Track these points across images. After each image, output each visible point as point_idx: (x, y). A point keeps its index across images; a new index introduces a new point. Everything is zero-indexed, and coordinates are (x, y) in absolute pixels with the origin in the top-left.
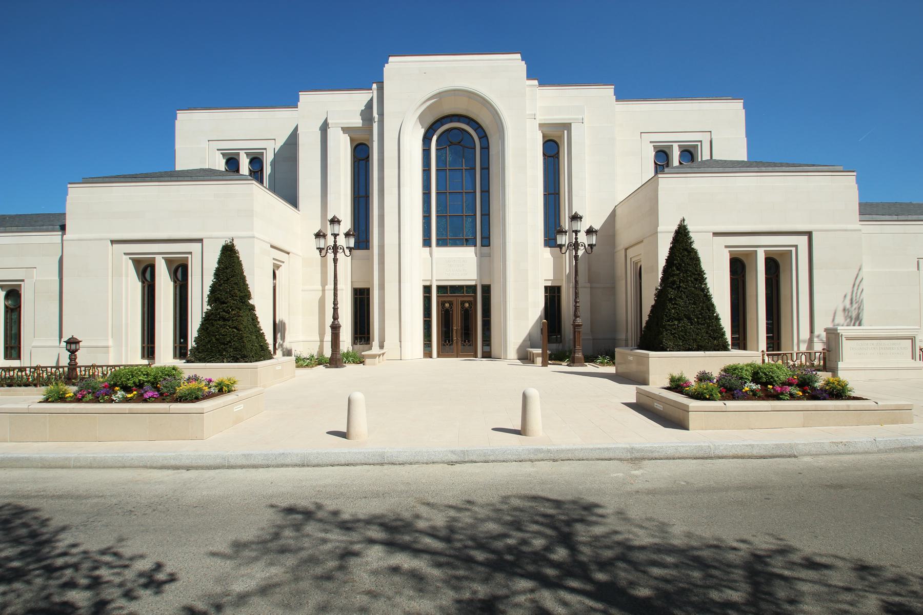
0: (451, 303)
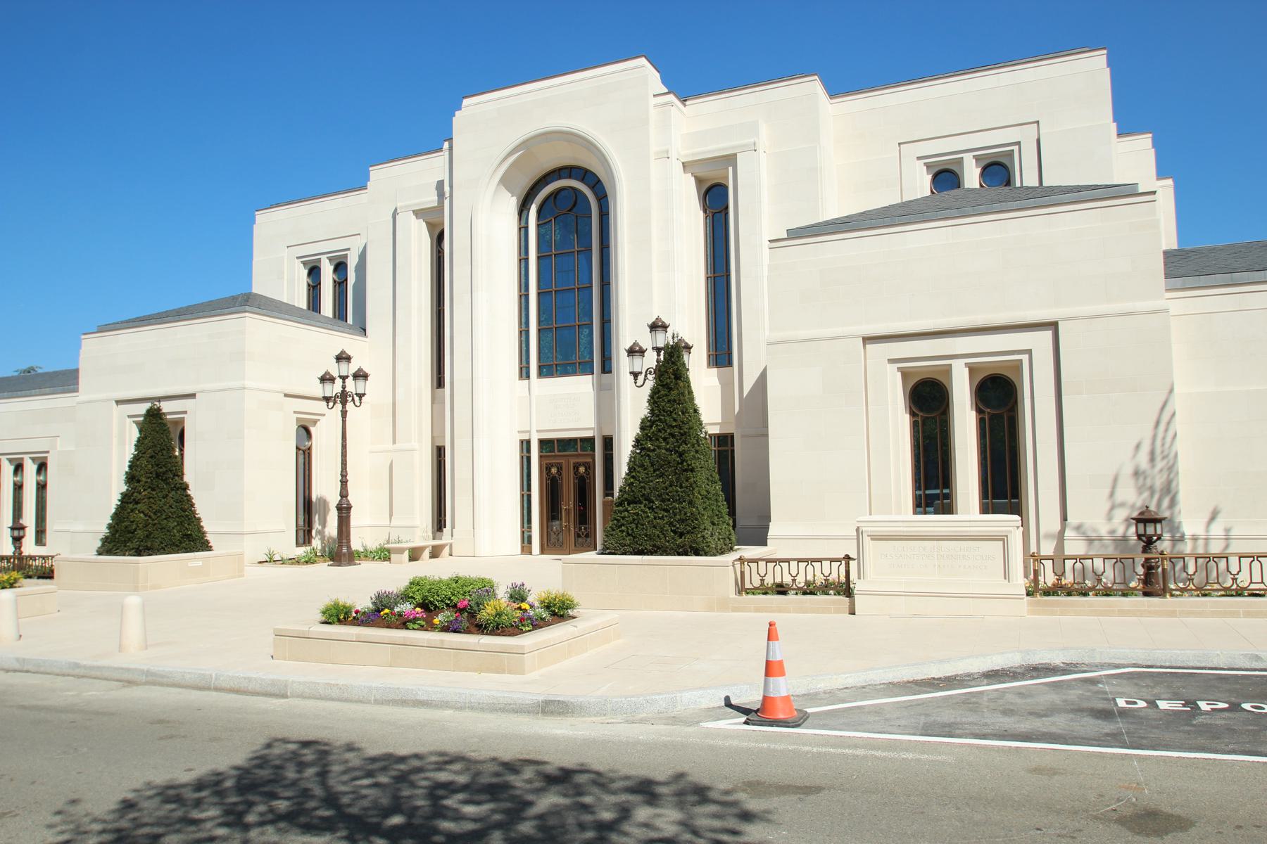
0: (560, 469)
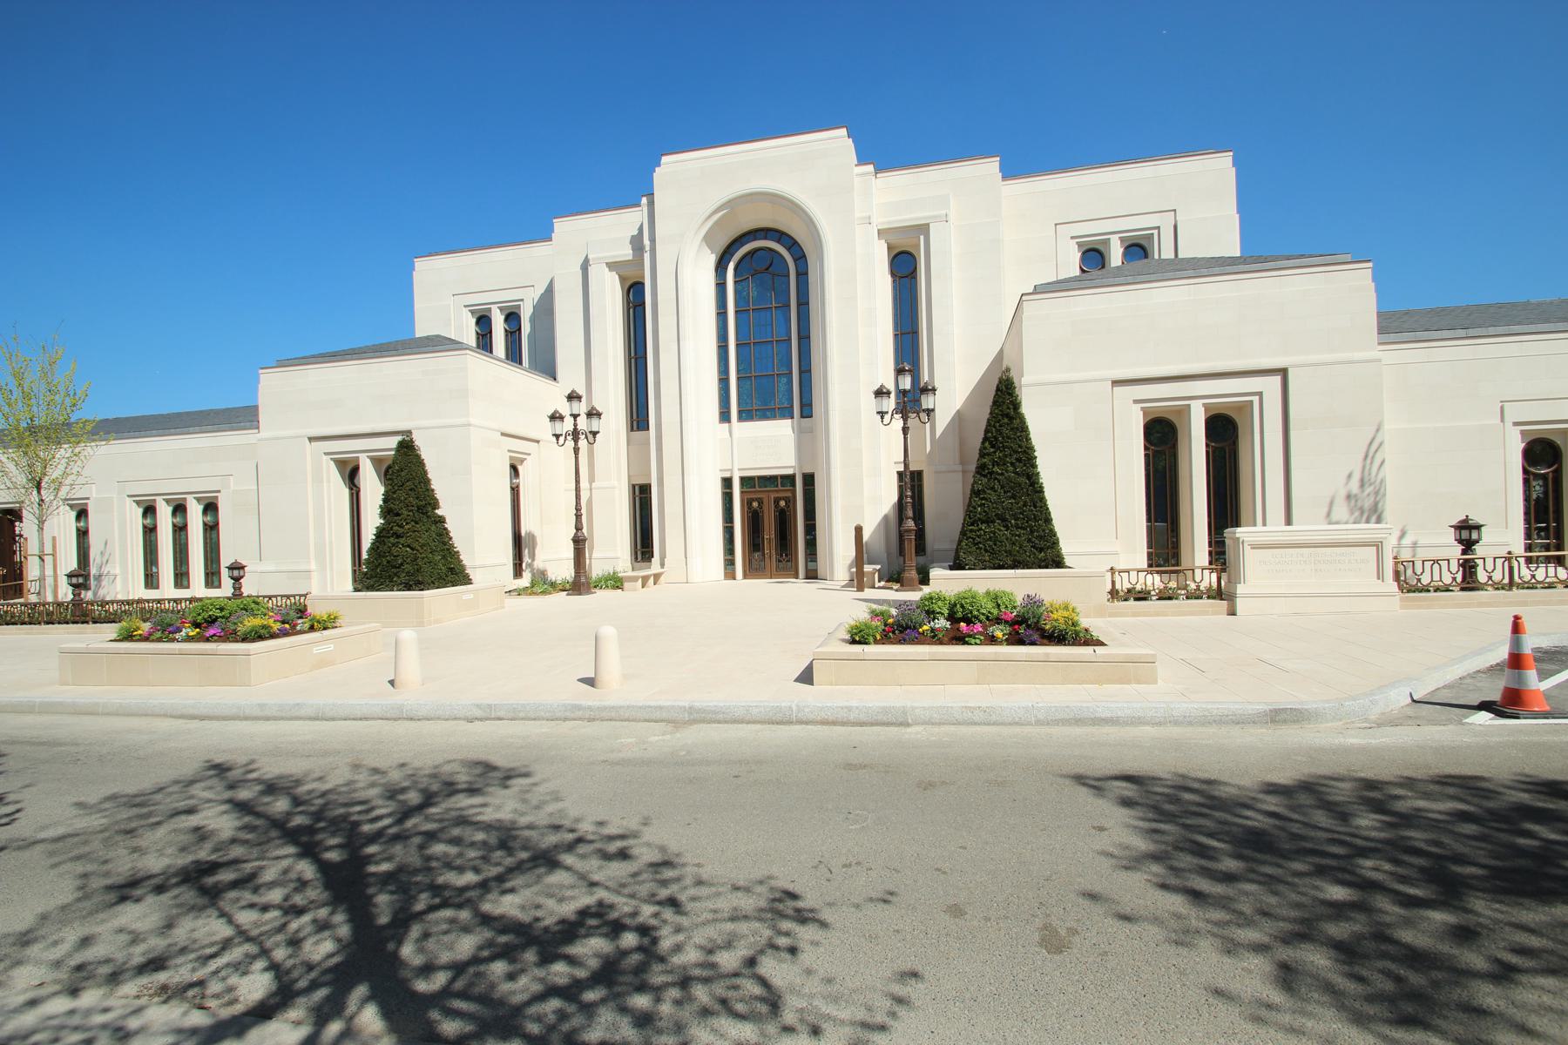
0: (760, 502)
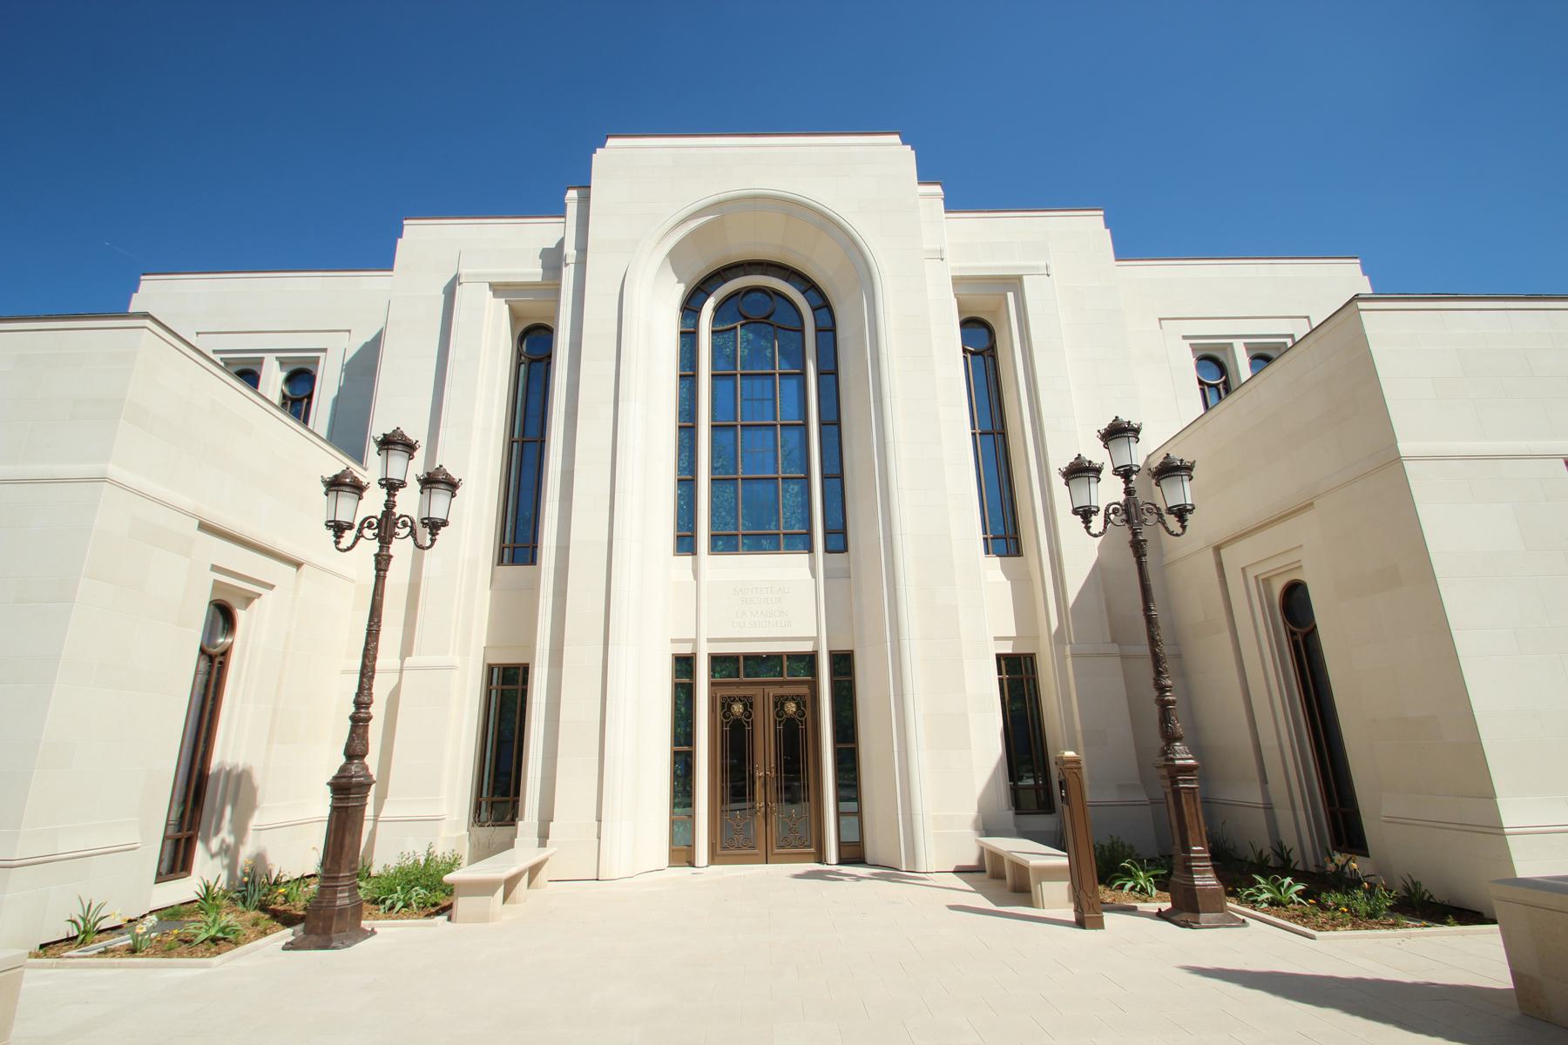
0: (748, 704)
